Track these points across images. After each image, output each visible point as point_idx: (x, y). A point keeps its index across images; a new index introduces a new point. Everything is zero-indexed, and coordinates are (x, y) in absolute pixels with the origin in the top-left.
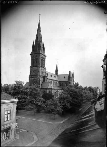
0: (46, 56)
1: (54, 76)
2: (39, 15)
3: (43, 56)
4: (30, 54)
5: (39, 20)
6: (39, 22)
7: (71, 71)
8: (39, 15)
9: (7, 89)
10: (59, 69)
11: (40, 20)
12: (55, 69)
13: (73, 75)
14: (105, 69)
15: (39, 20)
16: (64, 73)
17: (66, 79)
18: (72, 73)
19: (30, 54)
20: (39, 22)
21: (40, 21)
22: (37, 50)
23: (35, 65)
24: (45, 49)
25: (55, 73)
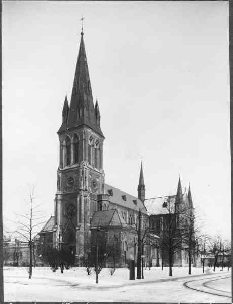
0: (105, 137)
1: (133, 201)
2: (82, 19)
3: (97, 137)
4: (58, 133)
5: (82, 34)
6: (82, 38)
7: (185, 192)
8: (82, 19)
9: (228, 265)
10: (146, 182)
11: (84, 32)
12: (137, 184)
13: (189, 196)
14: (163, 264)
15: (82, 34)
16: (161, 212)
17: (171, 209)
18: (187, 192)
19: (58, 133)
20: (82, 38)
21: (84, 36)
22: (79, 120)
23: (123, 221)
24: (100, 117)
25: (136, 195)
